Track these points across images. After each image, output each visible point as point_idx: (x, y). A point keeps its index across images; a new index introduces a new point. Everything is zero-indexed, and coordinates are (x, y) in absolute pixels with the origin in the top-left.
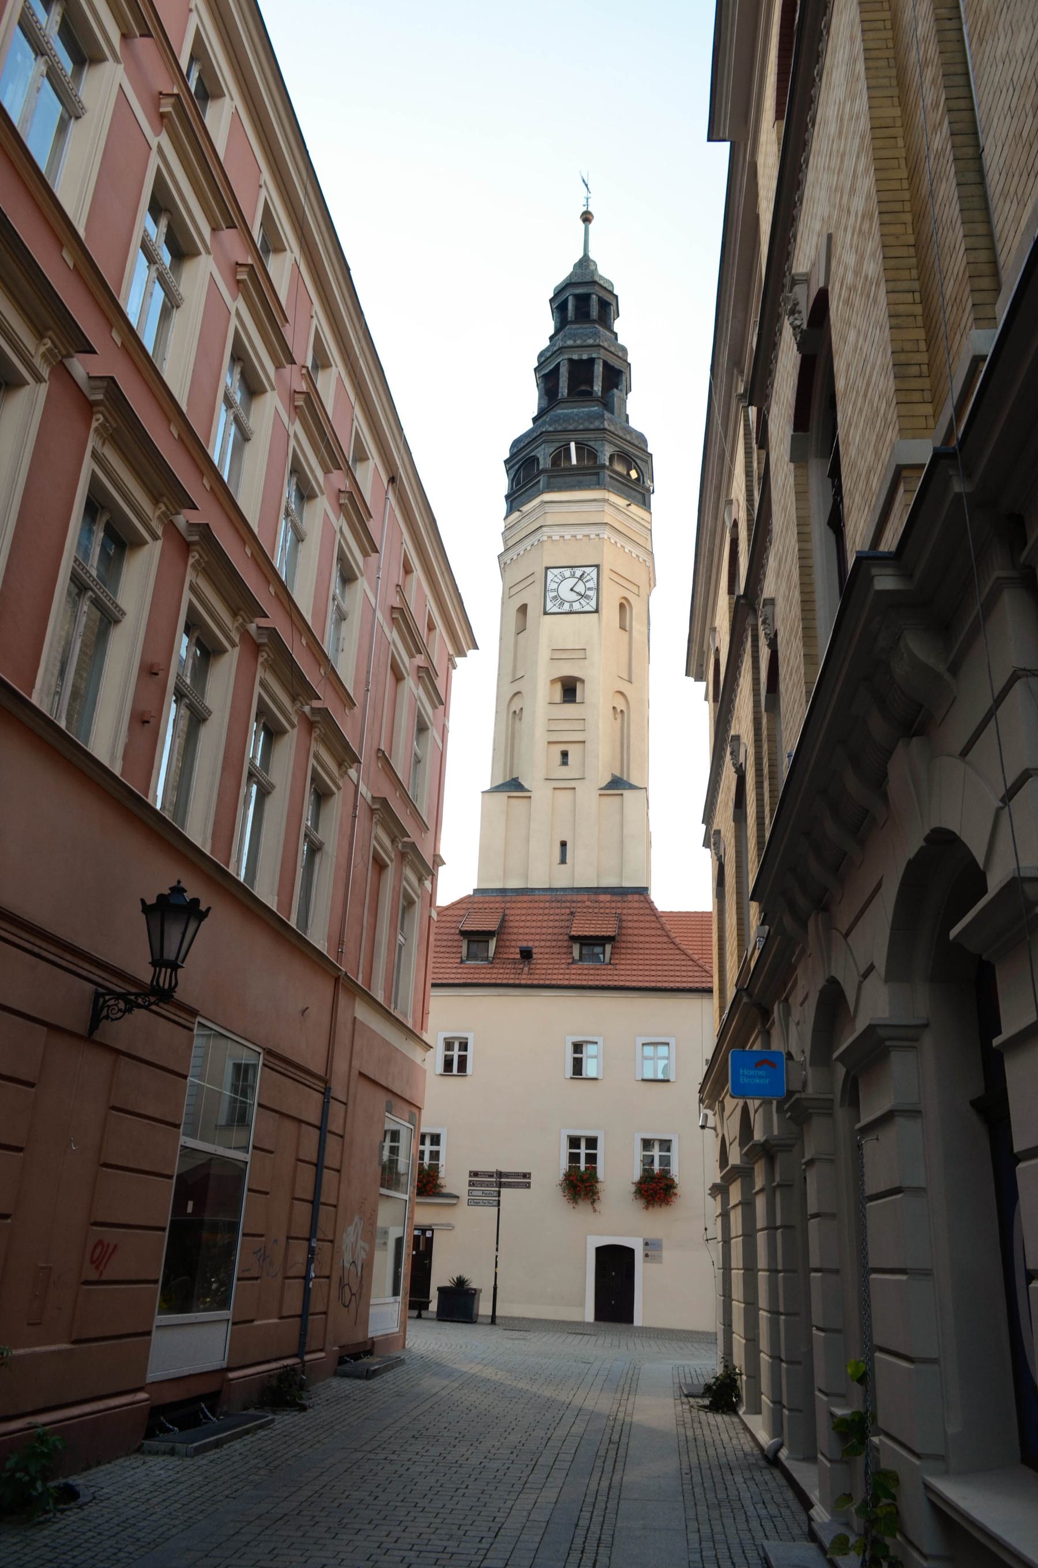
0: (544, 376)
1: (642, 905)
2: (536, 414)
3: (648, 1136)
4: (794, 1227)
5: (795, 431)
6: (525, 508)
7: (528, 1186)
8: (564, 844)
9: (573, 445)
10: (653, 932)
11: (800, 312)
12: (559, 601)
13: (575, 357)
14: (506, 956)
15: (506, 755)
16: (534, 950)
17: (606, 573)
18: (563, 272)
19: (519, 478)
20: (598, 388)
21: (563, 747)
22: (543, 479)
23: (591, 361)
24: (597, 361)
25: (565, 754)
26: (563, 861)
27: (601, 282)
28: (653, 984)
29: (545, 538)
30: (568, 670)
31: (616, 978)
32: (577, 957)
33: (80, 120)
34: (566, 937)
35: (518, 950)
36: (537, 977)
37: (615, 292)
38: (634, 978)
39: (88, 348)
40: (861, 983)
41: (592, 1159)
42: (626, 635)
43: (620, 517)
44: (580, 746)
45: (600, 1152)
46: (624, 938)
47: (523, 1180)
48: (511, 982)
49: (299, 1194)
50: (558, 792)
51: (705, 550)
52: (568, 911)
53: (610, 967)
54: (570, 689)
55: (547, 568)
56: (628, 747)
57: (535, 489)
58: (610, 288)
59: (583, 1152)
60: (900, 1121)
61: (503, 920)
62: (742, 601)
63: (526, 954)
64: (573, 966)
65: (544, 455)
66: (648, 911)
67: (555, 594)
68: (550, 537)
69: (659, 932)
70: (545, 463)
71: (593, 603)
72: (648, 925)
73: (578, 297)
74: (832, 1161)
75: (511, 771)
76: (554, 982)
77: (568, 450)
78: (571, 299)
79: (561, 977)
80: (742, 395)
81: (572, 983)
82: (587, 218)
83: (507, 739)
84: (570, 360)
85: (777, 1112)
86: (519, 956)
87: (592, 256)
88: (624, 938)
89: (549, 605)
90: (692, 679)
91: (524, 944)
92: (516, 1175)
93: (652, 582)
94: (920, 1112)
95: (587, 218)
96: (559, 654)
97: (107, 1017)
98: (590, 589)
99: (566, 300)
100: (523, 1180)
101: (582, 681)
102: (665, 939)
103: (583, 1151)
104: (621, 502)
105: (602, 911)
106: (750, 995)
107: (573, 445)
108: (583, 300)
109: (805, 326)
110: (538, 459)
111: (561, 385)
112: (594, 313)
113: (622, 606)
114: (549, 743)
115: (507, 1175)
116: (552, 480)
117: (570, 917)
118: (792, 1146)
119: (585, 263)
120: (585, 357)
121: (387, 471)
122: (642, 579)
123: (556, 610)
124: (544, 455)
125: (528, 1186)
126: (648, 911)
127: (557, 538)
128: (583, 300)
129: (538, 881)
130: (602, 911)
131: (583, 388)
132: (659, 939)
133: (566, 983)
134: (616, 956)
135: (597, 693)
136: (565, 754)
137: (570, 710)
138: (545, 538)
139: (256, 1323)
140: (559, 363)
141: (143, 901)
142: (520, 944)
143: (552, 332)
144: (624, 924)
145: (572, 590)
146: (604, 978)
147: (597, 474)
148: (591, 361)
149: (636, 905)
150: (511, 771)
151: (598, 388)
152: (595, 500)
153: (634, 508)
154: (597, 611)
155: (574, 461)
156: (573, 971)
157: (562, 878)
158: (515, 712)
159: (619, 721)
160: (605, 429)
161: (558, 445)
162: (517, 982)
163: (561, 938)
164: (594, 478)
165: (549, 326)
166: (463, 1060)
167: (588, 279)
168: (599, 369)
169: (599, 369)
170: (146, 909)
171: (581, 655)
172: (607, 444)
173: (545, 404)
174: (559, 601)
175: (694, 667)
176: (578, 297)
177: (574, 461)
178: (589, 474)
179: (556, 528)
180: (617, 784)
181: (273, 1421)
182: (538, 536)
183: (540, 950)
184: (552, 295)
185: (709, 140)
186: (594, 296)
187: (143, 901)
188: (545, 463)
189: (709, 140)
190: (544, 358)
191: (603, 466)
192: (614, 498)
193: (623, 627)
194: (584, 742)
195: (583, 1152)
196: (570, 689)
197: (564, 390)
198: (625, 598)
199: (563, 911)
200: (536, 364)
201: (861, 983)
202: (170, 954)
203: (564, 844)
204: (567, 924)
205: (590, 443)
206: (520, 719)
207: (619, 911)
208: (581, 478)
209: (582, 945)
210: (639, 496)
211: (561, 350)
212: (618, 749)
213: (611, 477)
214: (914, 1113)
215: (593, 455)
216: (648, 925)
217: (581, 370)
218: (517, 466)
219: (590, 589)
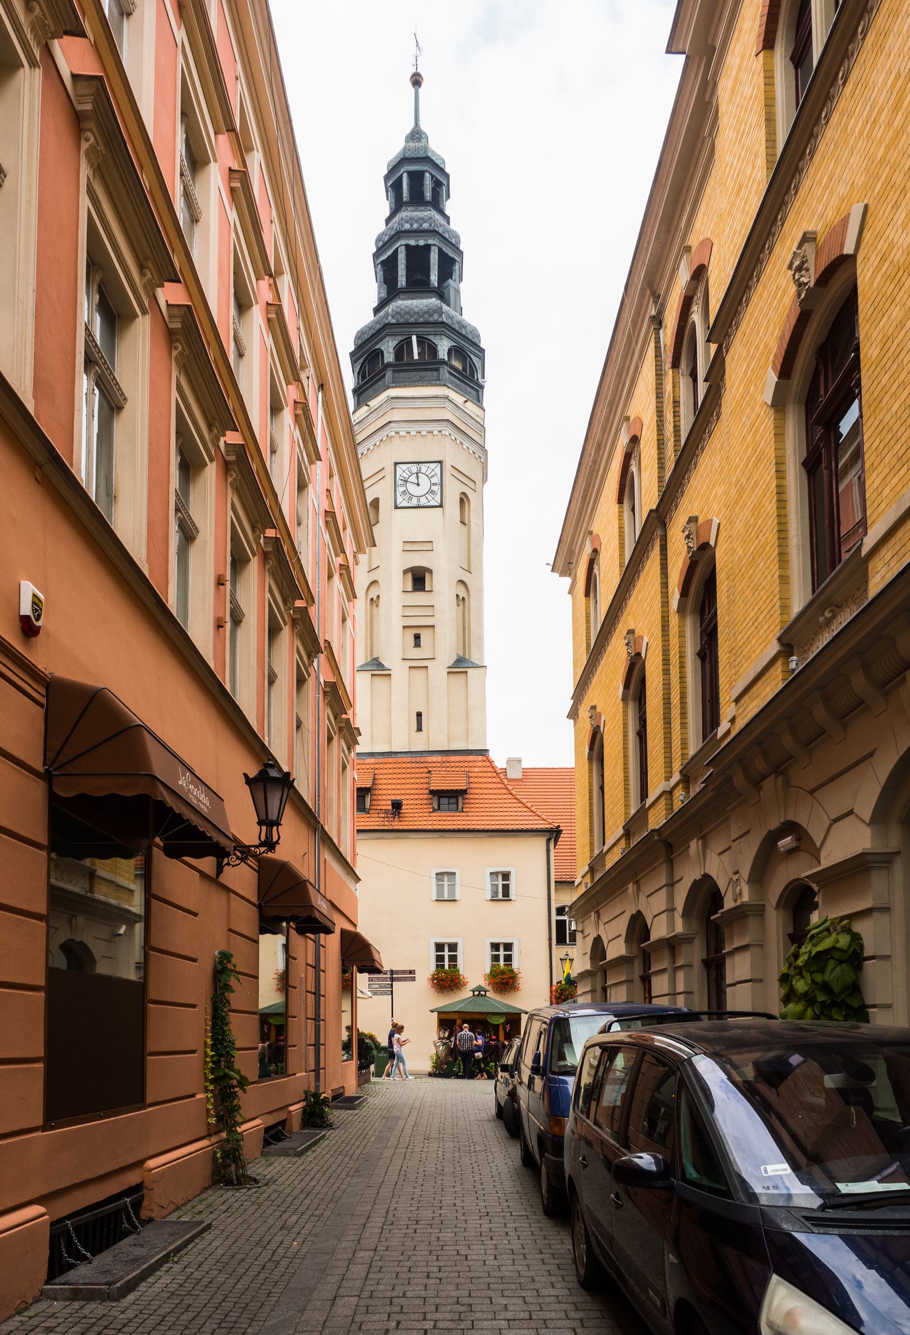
0: (382, 262)
1: (485, 764)
2: (376, 304)
3: (496, 941)
4: (692, 992)
5: (779, 378)
6: (374, 403)
7: (413, 979)
8: (419, 715)
9: (414, 338)
10: (495, 786)
11: (807, 270)
12: (408, 496)
13: (412, 243)
14: (379, 807)
15: (366, 637)
16: (404, 802)
17: (448, 470)
18: (395, 147)
19: (364, 372)
20: (434, 278)
21: (416, 631)
22: (389, 374)
23: (428, 247)
24: (433, 248)
25: (417, 637)
26: (419, 729)
27: (434, 158)
28: (498, 827)
29: (393, 434)
30: (417, 560)
31: (468, 822)
32: (436, 807)
33: (131, 17)
34: (427, 791)
35: (389, 803)
36: (406, 823)
37: (447, 170)
38: (517, 822)
39: (174, 278)
40: (831, 825)
41: (453, 959)
42: (465, 528)
43: (459, 414)
44: (430, 630)
45: (460, 953)
46: (472, 791)
47: (410, 975)
48: (386, 828)
49: (309, 989)
50: (413, 671)
51: (589, 461)
52: (426, 770)
53: (463, 814)
54: (419, 579)
55: (396, 464)
56: (469, 630)
57: (381, 382)
58: (442, 166)
59: (446, 952)
60: (875, 914)
61: (374, 779)
62: (654, 515)
63: (397, 806)
64: (434, 814)
65: (388, 348)
66: (490, 769)
67: (404, 488)
68: (397, 433)
69: (500, 786)
70: (389, 357)
71: (438, 498)
72: (490, 780)
73: (410, 174)
74: (761, 946)
75: (372, 651)
76: (420, 827)
77: (410, 343)
78: (405, 176)
79: (425, 823)
80: (654, 317)
81: (435, 827)
82: (416, 81)
83: (366, 623)
84: (408, 247)
85: (684, 915)
86: (390, 807)
87: (423, 127)
88: (472, 791)
89: (399, 499)
90: (556, 575)
91: (393, 798)
92: (404, 972)
93: (485, 478)
94: (889, 909)
95: (416, 81)
96: (410, 546)
97: (228, 864)
98: (435, 484)
99: (401, 177)
100: (410, 975)
101: (430, 571)
102: (505, 791)
103: (502, 953)
104: (459, 399)
105: (453, 769)
106: (660, 835)
107: (414, 338)
108: (416, 178)
109: (812, 284)
110: (382, 352)
111: (400, 274)
112: (428, 195)
113: (462, 501)
114: (404, 627)
115: (397, 972)
116: (396, 374)
117: (428, 775)
118: (693, 939)
119: (416, 135)
120: (421, 243)
121: (318, 380)
122: (477, 476)
123: (405, 504)
124: (388, 348)
125: (413, 979)
126: (490, 769)
127: (403, 434)
128: (416, 178)
129: (399, 746)
130: (453, 769)
131: (419, 277)
132: (500, 791)
133: (430, 827)
134: (467, 806)
135: (442, 585)
136: (417, 637)
137: (420, 598)
138: (393, 434)
139: (298, 1075)
140: (397, 249)
141: (245, 775)
142: (389, 797)
143: (388, 214)
144: (472, 780)
145: (418, 485)
146: (459, 823)
147: (437, 370)
148: (428, 247)
149: (480, 764)
150: (372, 651)
151: (434, 278)
152: (436, 397)
153: (469, 405)
154: (441, 506)
155: (416, 357)
156: (435, 818)
157: (419, 744)
158: (372, 599)
159: (461, 606)
160: (443, 323)
161: (401, 338)
162: (391, 827)
163: (422, 791)
164: (435, 373)
165: (384, 207)
166: (506, 889)
167: (421, 154)
168: (434, 257)
169: (434, 257)
170: (249, 781)
171: (428, 547)
172: (445, 338)
173: (384, 295)
174: (408, 496)
175: (560, 565)
176: (410, 174)
177: (416, 357)
178: (425, 368)
179: (403, 424)
180: (461, 665)
181: (324, 1135)
182: (386, 431)
183: (408, 802)
184: (386, 172)
185: (669, 51)
186: (427, 175)
187: (245, 775)
188: (389, 357)
189: (669, 51)
190: (383, 245)
191: (443, 362)
192: (453, 395)
193: (463, 522)
194: (433, 626)
195: (446, 952)
196: (419, 579)
197: (402, 281)
198: (464, 493)
199: (422, 770)
200: (375, 250)
201: (831, 825)
202: (273, 816)
203: (419, 715)
204: (426, 780)
205: (429, 337)
206: (377, 606)
207: (467, 769)
208: (422, 374)
209: (439, 797)
210: (474, 393)
211: (399, 234)
212: (461, 632)
213: (450, 373)
214: (886, 910)
215: (433, 350)
216: (490, 780)
217: (417, 257)
218: (361, 361)
219: (435, 484)
